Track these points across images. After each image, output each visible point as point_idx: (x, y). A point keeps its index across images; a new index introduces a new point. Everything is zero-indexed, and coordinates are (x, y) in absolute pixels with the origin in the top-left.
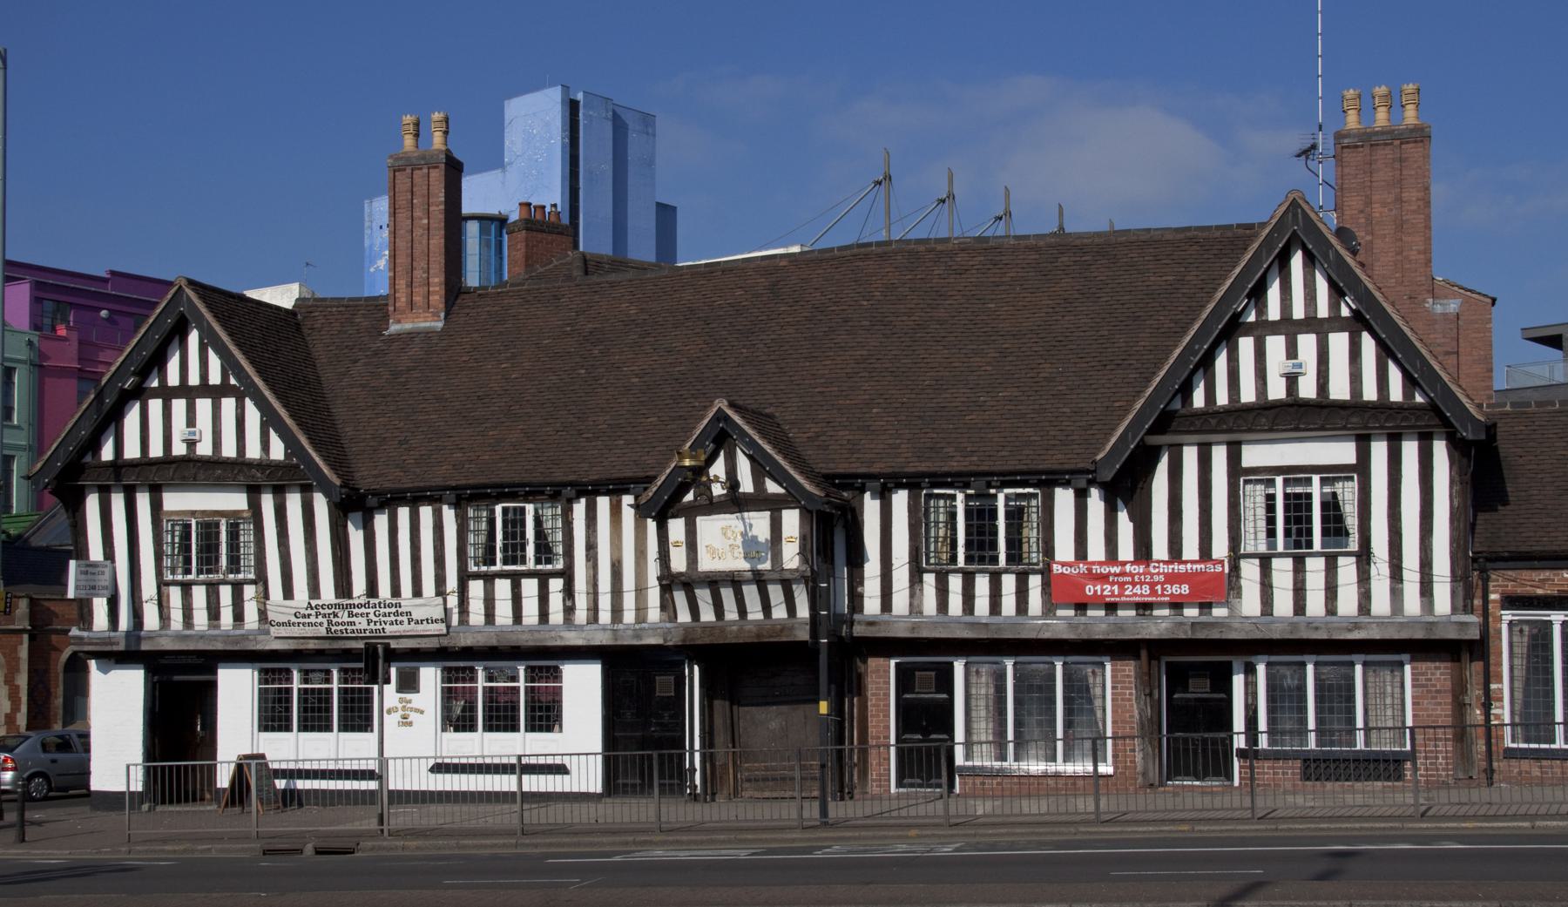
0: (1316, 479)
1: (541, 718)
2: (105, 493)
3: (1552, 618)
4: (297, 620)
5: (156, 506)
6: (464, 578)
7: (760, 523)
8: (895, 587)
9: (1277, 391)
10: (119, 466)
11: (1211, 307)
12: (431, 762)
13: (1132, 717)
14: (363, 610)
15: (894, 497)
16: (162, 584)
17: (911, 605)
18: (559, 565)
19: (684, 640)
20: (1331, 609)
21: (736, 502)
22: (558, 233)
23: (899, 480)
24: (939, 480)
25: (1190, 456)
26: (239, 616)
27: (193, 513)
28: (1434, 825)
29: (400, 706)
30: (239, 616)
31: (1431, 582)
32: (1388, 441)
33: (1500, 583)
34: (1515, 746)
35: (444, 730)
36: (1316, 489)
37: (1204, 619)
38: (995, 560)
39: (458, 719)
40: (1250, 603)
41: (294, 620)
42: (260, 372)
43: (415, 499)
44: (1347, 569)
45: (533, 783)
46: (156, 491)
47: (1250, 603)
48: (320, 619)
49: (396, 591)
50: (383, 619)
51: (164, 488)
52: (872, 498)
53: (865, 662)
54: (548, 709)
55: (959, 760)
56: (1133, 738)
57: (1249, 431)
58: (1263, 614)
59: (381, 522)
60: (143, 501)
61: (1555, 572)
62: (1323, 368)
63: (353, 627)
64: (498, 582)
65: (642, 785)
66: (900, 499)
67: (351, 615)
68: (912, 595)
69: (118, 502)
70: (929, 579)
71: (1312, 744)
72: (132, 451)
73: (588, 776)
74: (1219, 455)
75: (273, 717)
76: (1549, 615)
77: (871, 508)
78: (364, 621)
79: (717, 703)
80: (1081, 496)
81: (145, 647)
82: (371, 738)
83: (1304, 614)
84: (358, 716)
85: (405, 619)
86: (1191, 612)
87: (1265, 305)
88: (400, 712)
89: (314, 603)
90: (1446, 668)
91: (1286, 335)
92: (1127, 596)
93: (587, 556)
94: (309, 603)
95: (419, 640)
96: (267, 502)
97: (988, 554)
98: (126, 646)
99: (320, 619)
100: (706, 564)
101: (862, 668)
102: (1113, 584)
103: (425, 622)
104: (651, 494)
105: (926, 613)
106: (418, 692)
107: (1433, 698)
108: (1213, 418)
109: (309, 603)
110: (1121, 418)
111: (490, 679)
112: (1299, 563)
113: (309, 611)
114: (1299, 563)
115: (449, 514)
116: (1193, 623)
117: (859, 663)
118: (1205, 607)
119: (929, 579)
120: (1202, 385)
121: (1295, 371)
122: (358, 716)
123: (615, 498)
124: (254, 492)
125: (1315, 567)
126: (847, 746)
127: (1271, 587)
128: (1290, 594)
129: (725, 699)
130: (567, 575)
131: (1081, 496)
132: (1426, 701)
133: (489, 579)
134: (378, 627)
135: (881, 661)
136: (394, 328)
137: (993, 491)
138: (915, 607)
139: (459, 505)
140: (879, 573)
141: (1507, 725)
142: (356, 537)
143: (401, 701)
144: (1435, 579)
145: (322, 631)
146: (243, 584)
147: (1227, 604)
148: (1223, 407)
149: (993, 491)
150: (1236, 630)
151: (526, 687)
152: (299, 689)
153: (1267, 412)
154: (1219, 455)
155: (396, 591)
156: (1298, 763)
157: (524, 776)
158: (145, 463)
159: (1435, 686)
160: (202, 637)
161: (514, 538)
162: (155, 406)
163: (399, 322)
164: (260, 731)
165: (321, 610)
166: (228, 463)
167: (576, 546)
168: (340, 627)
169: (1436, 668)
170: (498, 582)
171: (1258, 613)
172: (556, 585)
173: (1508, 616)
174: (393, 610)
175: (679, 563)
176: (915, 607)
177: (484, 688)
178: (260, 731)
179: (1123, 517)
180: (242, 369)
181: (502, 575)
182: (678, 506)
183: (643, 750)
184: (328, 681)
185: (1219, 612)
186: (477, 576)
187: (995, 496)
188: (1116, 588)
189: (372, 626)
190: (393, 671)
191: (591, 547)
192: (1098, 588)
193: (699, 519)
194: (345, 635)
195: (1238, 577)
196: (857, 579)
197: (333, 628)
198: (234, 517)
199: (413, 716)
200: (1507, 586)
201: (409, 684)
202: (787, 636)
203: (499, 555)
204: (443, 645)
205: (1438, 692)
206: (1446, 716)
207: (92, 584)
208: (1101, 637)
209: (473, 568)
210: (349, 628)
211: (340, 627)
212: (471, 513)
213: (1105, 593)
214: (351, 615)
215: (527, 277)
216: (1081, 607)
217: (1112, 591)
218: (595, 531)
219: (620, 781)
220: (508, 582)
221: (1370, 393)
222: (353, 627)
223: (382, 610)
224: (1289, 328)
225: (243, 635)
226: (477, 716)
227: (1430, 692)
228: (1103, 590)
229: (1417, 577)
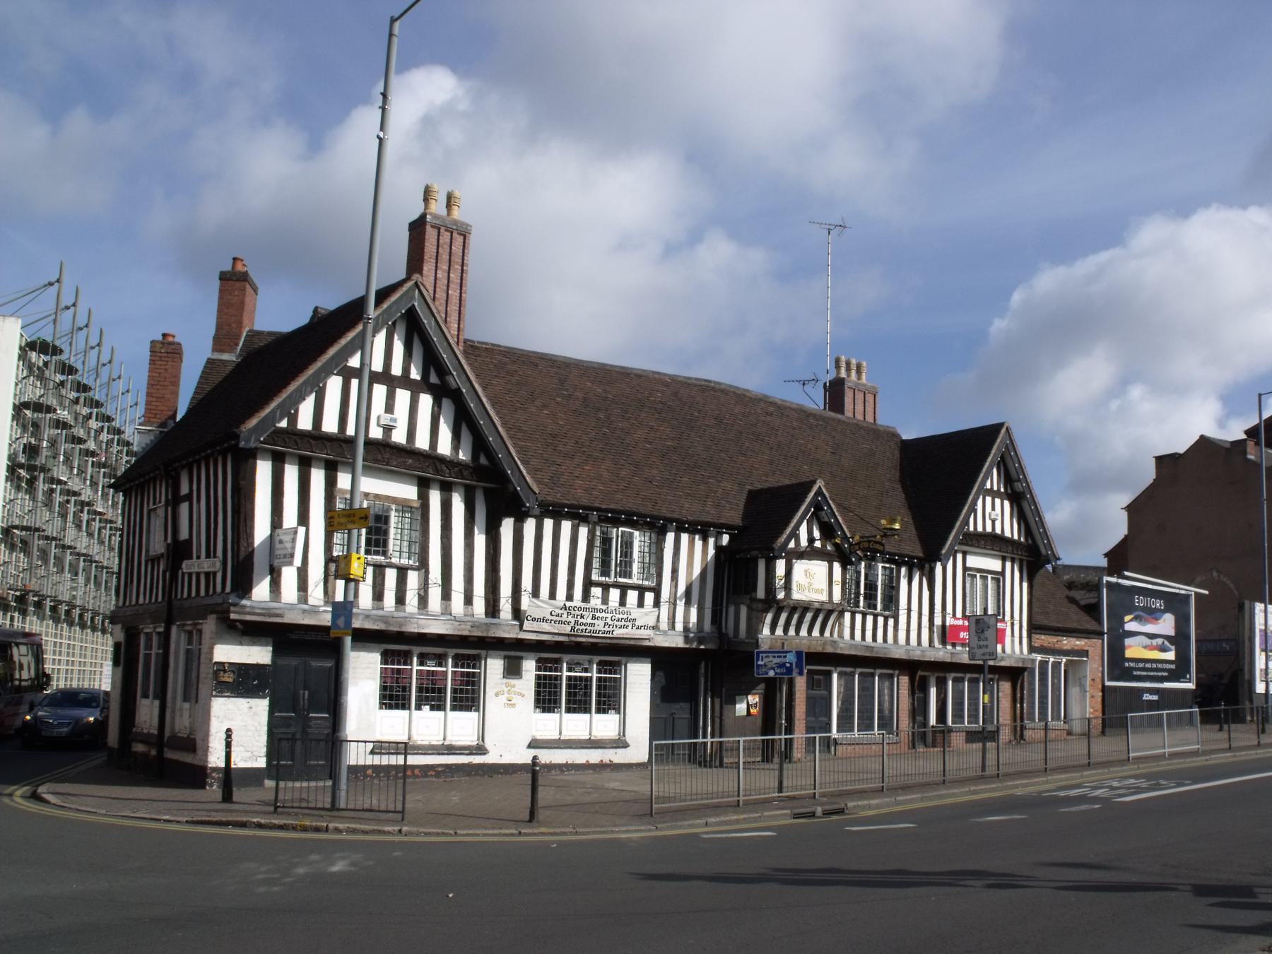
1: (604, 702)
2: (279, 462)
4: (551, 618)
5: (331, 483)
6: (588, 584)
8: (912, 628)
9: (989, 529)
14: (603, 615)
26: (400, 600)
29: (506, 690)
30: (400, 600)
32: (273, 461)
37: (954, 651)
38: (875, 608)
39: (546, 700)
46: (331, 470)
48: (570, 618)
50: (616, 623)
51: (340, 467)
52: (699, 540)
59: (530, 526)
60: (318, 477)
63: (592, 628)
64: (612, 590)
65: (668, 755)
67: (594, 617)
69: (291, 473)
73: (638, 750)
75: (393, 696)
78: (601, 623)
82: (471, 717)
84: (468, 698)
85: (630, 624)
89: (568, 604)
93: (672, 577)
94: (565, 605)
96: (435, 497)
97: (872, 602)
99: (570, 618)
100: (796, 595)
103: (642, 628)
104: (783, 540)
106: (521, 678)
109: (565, 605)
113: (563, 611)
121: (391, 424)
122: (468, 698)
123: (692, 536)
124: (424, 486)
126: (64, 676)
128: (905, 632)
130: (657, 591)
133: (606, 587)
134: (611, 629)
140: (900, 617)
145: (567, 629)
146: (385, 567)
156: (964, 734)
158: (316, 437)
160: (368, 617)
161: (626, 557)
165: (572, 612)
166: (397, 449)
167: (431, 545)
168: (583, 627)
170: (612, 590)
171: (916, 645)
172: (891, 622)
174: (625, 616)
181: (616, 585)
186: (598, 584)
189: (606, 629)
191: (675, 571)
194: (583, 634)
197: (577, 627)
198: (404, 505)
199: (516, 699)
201: (513, 670)
203: (382, 541)
208: (916, 659)
209: (595, 577)
210: (589, 628)
211: (583, 627)
214: (594, 617)
218: (678, 559)
220: (636, 593)
221: (422, 442)
222: (592, 628)
223: (617, 616)
226: (566, 696)
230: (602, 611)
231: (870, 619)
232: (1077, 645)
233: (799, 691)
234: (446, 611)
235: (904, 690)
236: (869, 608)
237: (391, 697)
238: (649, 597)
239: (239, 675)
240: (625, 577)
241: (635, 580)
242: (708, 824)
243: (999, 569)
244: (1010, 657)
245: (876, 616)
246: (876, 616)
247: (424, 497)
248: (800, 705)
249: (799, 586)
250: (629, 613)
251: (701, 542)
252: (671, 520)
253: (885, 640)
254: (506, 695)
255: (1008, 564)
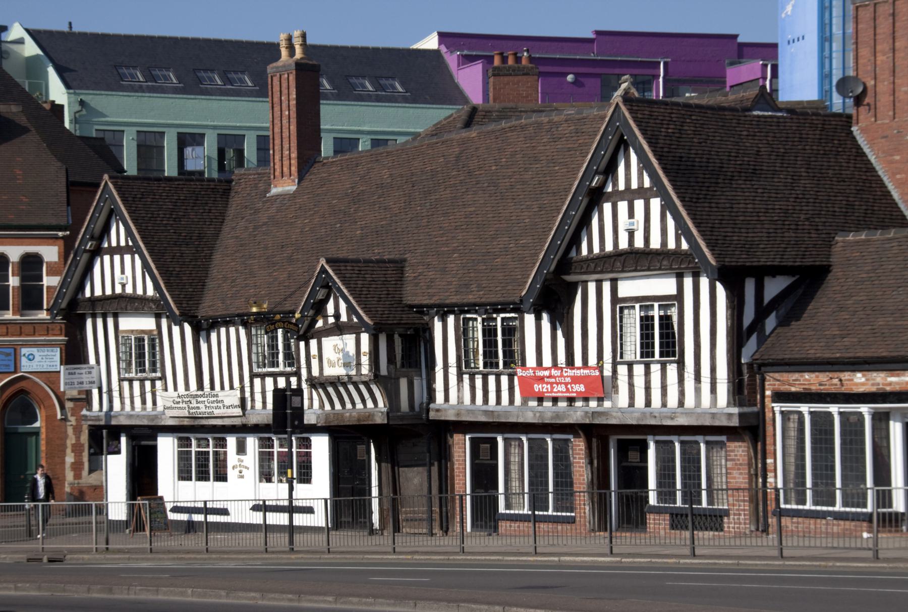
0: (656, 305)
2: (94, 316)
3: (830, 410)
7: (350, 339)
10: (93, 301)
11: (576, 183)
12: (251, 504)
13: (584, 480)
15: (449, 319)
16: (121, 380)
17: (458, 397)
18: (159, 374)
19: (325, 423)
20: (664, 405)
21: (339, 329)
22: (524, 74)
23: (495, 307)
24: (472, 307)
25: (592, 287)
27: (132, 331)
28: (766, 562)
31: (715, 383)
33: (772, 383)
34: (788, 506)
35: (261, 481)
36: (656, 313)
37: (599, 409)
40: (623, 399)
41: (174, 406)
42: (142, 238)
43: (227, 324)
44: (672, 370)
45: (212, 518)
47: (623, 399)
49: (212, 387)
51: (119, 315)
53: (452, 437)
54: (281, 473)
55: (502, 509)
56: (584, 492)
57: (623, 271)
58: (629, 406)
60: (110, 322)
61: (801, 374)
62: (647, 225)
66: (451, 319)
67: (198, 402)
68: (459, 390)
70: (466, 377)
71: (679, 503)
72: (98, 292)
74: (606, 287)
76: (799, 407)
77: (438, 325)
79: (383, 465)
80: (538, 319)
81: (114, 422)
83: (633, 406)
86: (593, 404)
87: (617, 180)
88: (239, 469)
90: (745, 447)
91: (644, 199)
92: (555, 392)
95: (232, 419)
97: (494, 360)
98: (106, 422)
100: (329, 372)
101: (450, 441)
102: (547, 383)
105: (465, 404)
107: (739, 469)
108: (593, 263)
110: (533, 267)
111: (199, 446)
112: (647, 366)
114: (647, 366)
115: (242, 331)
116: (593, 412)
117: (449, 438)
118: (600, 400)
119: (466, 377)
120: (586, 239)
125: (655, 369)
127: (633, 386)
129: (388, 463)
131: (538, 319)
132: (735, 472)
135: (460, 436)
136: (274, 191)
137: (495, 316)
138: (460, 400)
139: (245, 325)
141: (899, 488)
142: (204, 347)
143: (240, 460)
144: (718, 381)
145: (185, 413)
147: (610, 399)
148: (610, 252)
149: (495, 316)
150: (615, 418)
151: (214, 451)
152: (196, 452)
153: (620, 258)
154: (606, 287)
155: (212, 387)
157: (267, 513)
158: (104, 299)
159: (738, 460)
161: (273, 350)
162: (107, 258)
163: (276, 186)
164: (179, 480)
168: (194, 411)
169: (740, 447)
171: (627, 406)
173: (778, 407)
174: (215, 399)
175: (315, 372)
176: (460, 400)
177: (196, 452)
178: (179, 480)
179: (559, 333)
180: (135, 238)
182: (312, 331)
183: (353, 496)
184: (208, 446)
185: (607, 404)
187: (496, 319)
188: (549, 386)
189: (208, 410)
190: (293, 438)
192: (540, 386)
193: (323, 339)
195: (617, 379)
196: (431, 380)
199: (245, 472)
200: (775, 385)
202: (372, 420)
204: (244, 423)
205: (741, 464)
206: (745, 483)
207: (80, 380)
209: (256, 370)
212: (253, 331)
213: (545, 390)
214: (198, 402)
215: (522, 114)
216: (540, 400)
217: (547, 389)
219: (343, 519)
224: (630, 195)
225: (155, 415)
227: (736, 464)
228: (543, 388)
229: (709, 380)
230: (201, 396)
231: (492, 379)
232: (890, 384)
233: (457, 460)
234: (144, 409)
235: (580, 458)
236: (491, 367)
237: (717, 525)
238: (159, 384)
239: (775, 515)
240: (273, 367)
241: (281, 368)
242: (153, 551)
243: (673, 291)
244: (689, 413)
245: (498, 376)
246: (498, 376)
247: (159, 326)
248: (459, 476)
249: (329, 361)
250: (217, 396)
251: (440, 323)
252: (431, 307)
253: (499, 401)
254: (239, 469)
255: (688, 282)
